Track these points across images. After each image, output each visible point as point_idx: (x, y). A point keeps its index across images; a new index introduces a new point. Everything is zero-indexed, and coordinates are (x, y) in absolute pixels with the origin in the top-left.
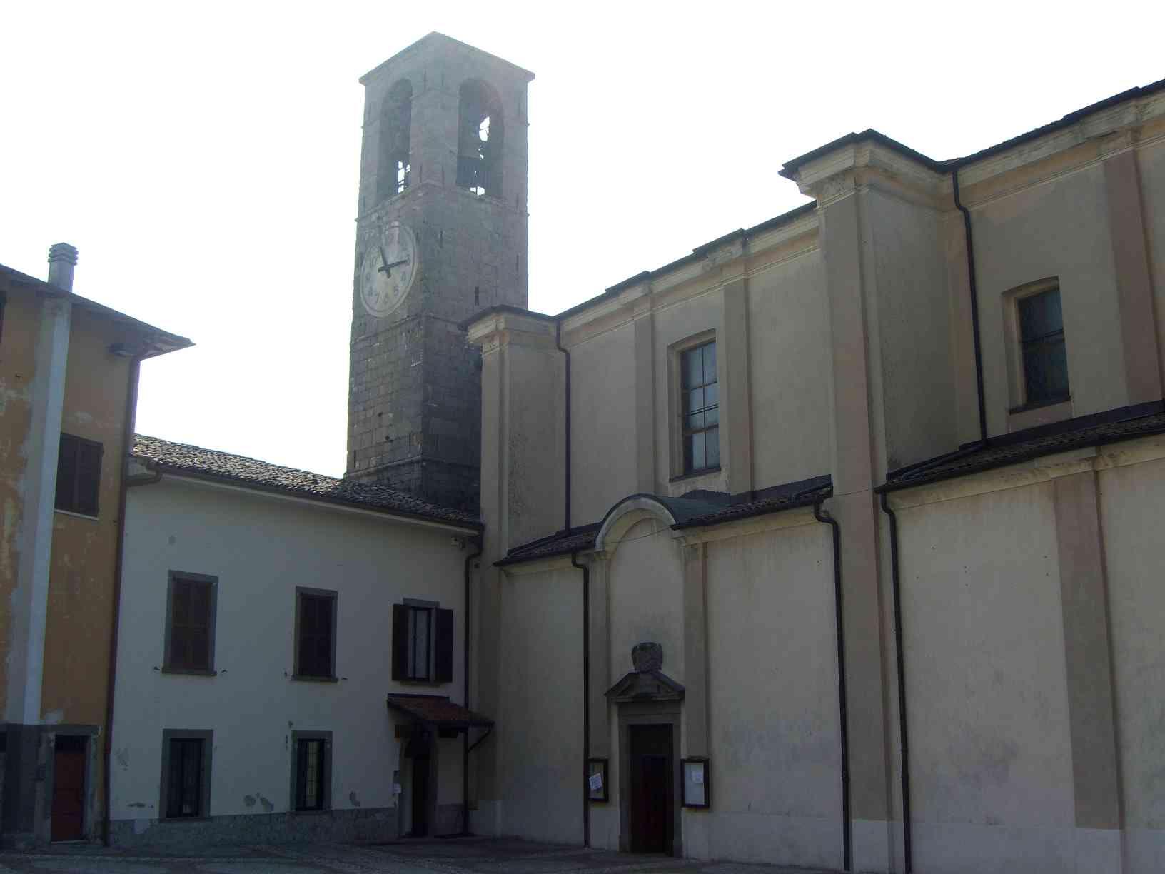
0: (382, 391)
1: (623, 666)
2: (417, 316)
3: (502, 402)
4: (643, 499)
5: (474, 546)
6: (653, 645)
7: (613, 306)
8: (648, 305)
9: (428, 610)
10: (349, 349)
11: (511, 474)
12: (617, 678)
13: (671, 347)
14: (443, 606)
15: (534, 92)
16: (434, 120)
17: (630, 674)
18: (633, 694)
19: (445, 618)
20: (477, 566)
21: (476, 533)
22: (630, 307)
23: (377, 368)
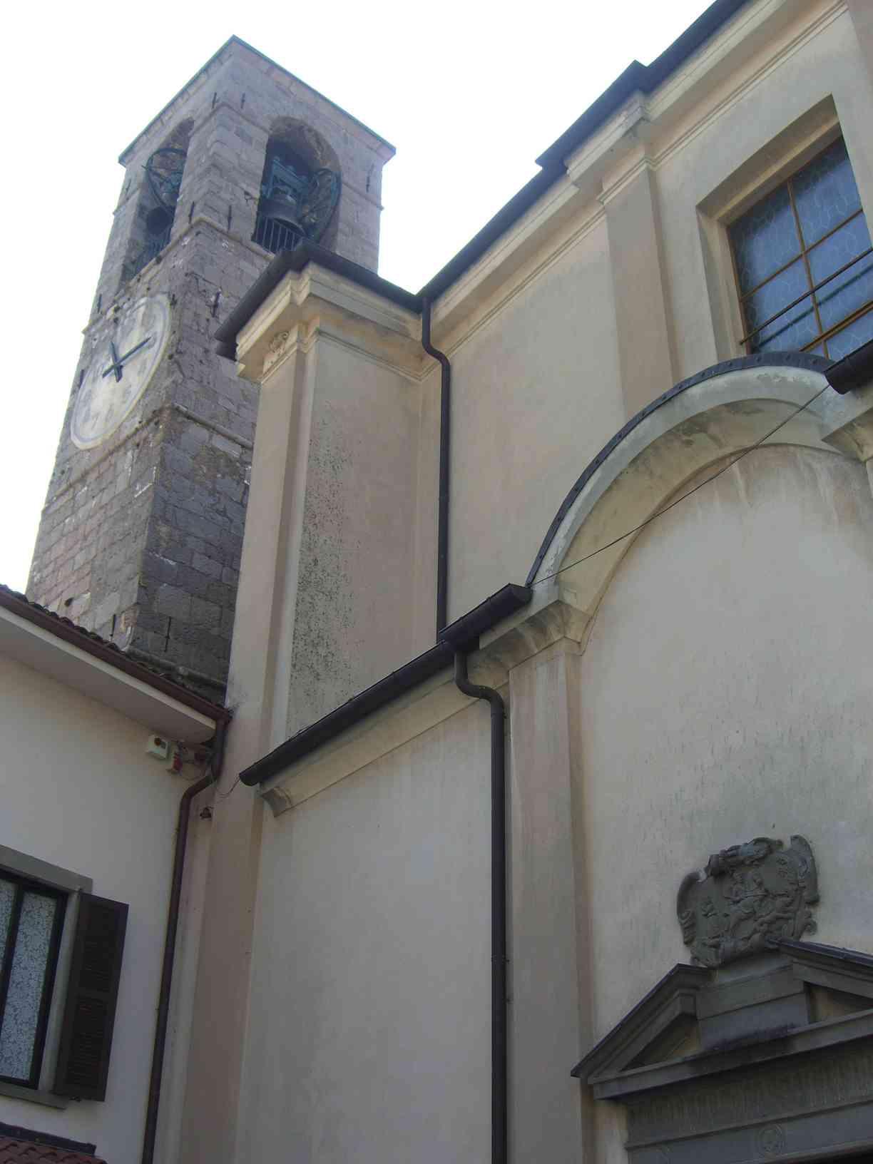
0: (80, 559)
1: (637, 947)
2: (157, 413)
3: (298, 396)
4: (695, 391)
5: (200, 759)
6: (768, 848)
7: (562, 195)
8: (641, 154)
9: (59, 896)
10: (39, 518)
11: (304, 584)
12: (617, 997)
13: (705, 208)
14: (101, 890)
15: (392, 179)
16: (230, 176)
17: (680, 968)
18: (693, 1050)
19: (103, 925)
20: (207, 814)
21: (209, 723)
22: (594, 183)
23: (76, 529)
